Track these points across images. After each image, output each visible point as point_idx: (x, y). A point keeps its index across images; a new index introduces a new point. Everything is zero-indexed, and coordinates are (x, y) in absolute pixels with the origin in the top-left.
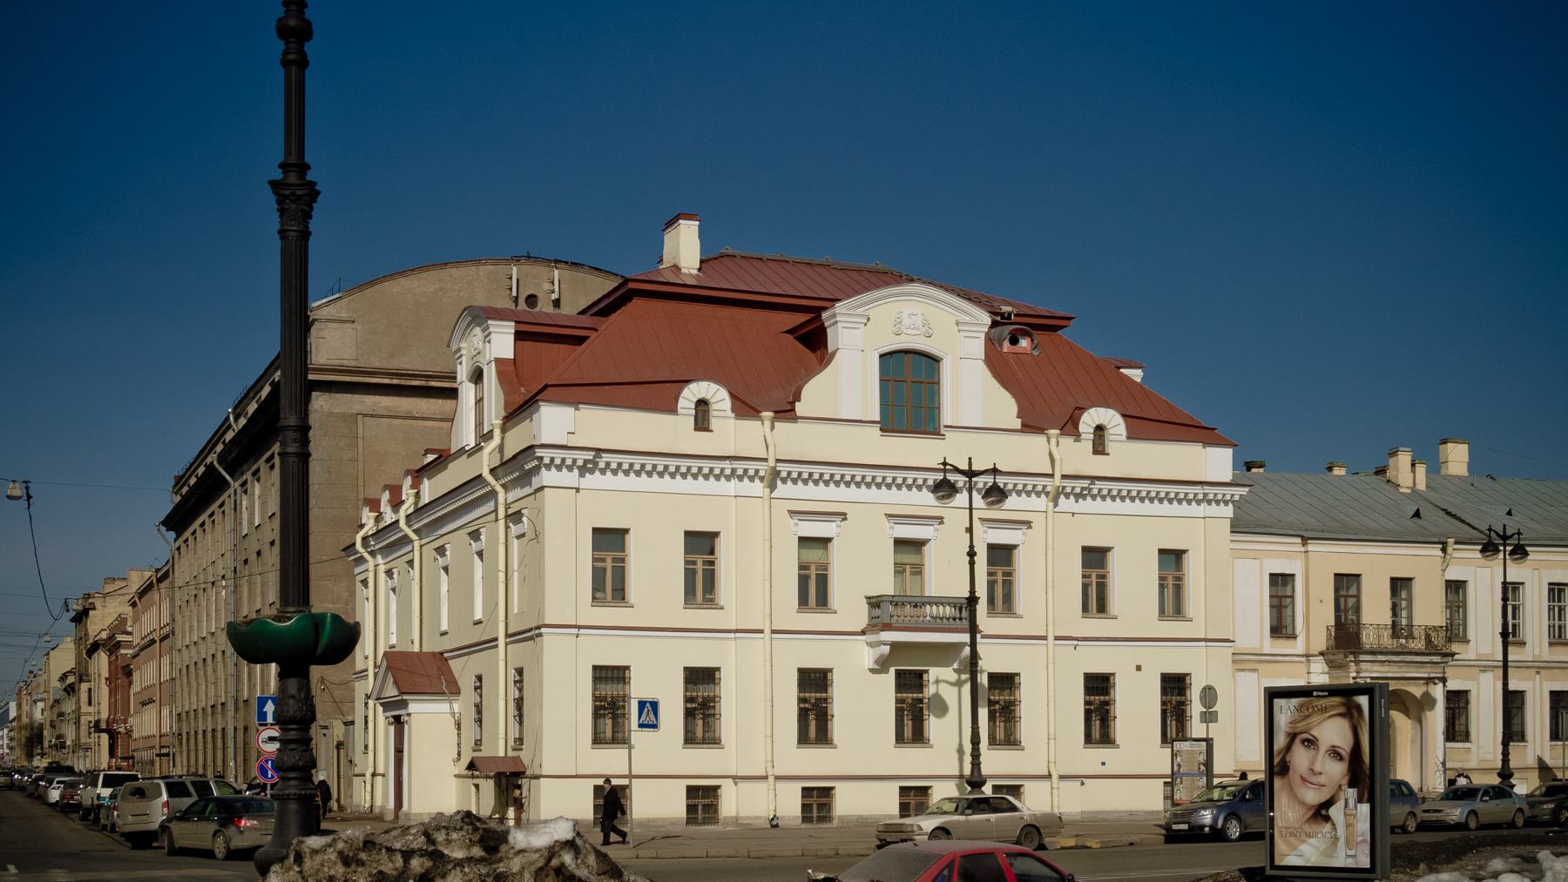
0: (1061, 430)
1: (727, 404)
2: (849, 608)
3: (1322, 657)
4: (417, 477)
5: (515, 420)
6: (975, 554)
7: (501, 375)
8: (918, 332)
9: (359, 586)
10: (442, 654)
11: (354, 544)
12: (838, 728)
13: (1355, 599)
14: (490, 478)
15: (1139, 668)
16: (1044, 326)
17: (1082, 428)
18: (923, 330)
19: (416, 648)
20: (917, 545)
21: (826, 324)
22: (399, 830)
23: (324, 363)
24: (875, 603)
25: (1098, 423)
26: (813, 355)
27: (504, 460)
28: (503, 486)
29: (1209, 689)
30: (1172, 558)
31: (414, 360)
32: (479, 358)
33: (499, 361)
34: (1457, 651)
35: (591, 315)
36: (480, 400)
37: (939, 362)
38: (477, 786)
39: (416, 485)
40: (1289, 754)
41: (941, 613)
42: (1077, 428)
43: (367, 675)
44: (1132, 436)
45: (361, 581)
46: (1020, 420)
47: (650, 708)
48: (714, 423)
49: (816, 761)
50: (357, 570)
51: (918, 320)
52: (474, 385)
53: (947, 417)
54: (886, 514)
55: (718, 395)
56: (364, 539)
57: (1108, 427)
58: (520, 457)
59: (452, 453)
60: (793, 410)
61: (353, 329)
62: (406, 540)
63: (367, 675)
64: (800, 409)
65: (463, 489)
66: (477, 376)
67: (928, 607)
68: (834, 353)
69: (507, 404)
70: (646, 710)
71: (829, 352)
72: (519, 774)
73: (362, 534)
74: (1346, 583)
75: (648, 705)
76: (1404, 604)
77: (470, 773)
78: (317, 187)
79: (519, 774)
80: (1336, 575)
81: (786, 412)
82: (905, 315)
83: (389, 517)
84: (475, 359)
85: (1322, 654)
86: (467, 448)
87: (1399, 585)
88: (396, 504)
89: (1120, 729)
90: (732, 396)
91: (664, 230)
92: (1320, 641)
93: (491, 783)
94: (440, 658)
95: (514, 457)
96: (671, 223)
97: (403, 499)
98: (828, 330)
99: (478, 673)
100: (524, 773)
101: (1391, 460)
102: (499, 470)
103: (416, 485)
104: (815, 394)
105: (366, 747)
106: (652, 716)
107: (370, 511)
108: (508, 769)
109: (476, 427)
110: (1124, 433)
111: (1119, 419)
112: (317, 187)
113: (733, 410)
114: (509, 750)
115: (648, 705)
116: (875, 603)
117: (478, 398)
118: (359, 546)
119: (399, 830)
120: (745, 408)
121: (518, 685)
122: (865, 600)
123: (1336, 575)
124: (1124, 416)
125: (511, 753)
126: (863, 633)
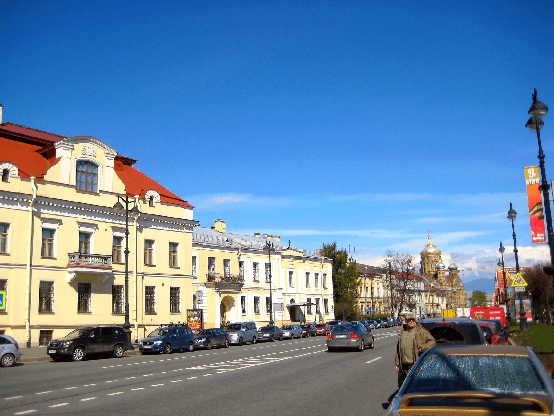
1: (17, 172)
2: (62, 259)
8: (91, 155)
12: (54, 307)
17: (146, 196)
18: (93, 154)
20: (52, 231)
21: (56, 148)
22: (239, 285)
25: (151, 195)
31: (28, 173)
37: (97, 167)
42: (144, 196)
44: (162, 202)
46: (125, 192)
49: (46, 320)
54: (77, 222)
57: (153, 196)
60: (43, 178)
64: (46, 178)
68: (60, 159)
71: (57, 158)
76: (242, 269)
78: (338, 249)
81: (40, 179)
82: (86, 148)
87: (226, 262)
89: (156, 308)
90: (19, 170)
92: (204, 279)
98: (57, 150)
104: (51, 174)
110: (160, 200)
111: (157, 195)
112: (338, 249)
113: (19, 175)
116: (71, 256)
119: (239, 285)
120: (24, 176)
124: (160, 195)
126: (67, 267)
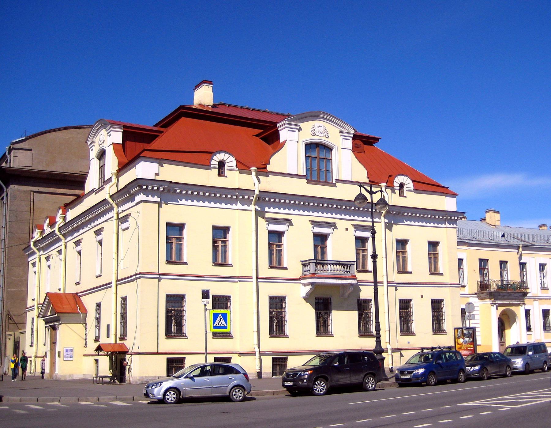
0: (386, 183)
1: (234, 164)
3: (476, 295)
4: (65, 209)
5: (125, 170)
6: (375, 232)
7: (115, 151)
8: (323, 135)
9: (30, 266)
10: (77, 294)
11: (30, 246)
12: (288, 328)
13: (487, 270)
14: (110, 200)
15: (422, 297)
16: (369, 141)
19: (62, 291)
21: (279, 129)
23: (17, 167)
24: (305, 264)
25: (401, 182)
26: (270, 146)
27: (119, 190)
28: (116, 204)
29: (470, 304)
30: (433, 245)
32: (103, 145)
33: (114, 144)
34: (529, 292)
35: (159, 127)
36: (102, 166)
38: (97, 361)
39: (64, 213)
40: (15, 371)
41: (332, 268)
43: (34, 308)
45: (32, 264)
47: (221, 317)
48: (227, 173)
50: (30, 259)
51: (322, 129)
52: (99, 161)
53: (335, 176)
55: (231, 161)
56: (35, 242)
58: (128, 187)
59: (85, 194)
60: (265, 168)
61: (31, 153)
62: (59, 240)
63: (34, 308)
64: (269, 168)
65: (93, 209)
66: (102, 155)
67: (329, 265)
68: (285, 142)
69: (119, 164)
70: (219, 318)
72: (126, 353)
73: (34, 240)
74: (483, 263)
75: (220, 315)
77: (97, 353)
79: (126, 353)
80: (480, 259)
81: (263, 171)
82: (316, 127)
83: (48, 230)
84: (101, 146)
85: (476, 294)
86: (95, 190)
87: (503, 264)
88: (52, 224)
89: (415, 327)
91: (194, 90)
92: (475, 288)
93: (108, 358)
94: (76, 297)
95: (125, 187)
96: (197, 86)
97: (57, 221)
98: (280, 132)
99: (98, 302)
100: (127, 352)
101: (486, 214)
102: (115, 196)
103: (64, 213)
105: (32, 343)
106: (223, 322)
107: (38, 230)
108: (117, 349)
109: (99, 180)
110: (412, 187)
114: (118, 340)
115: (220, 315)
116: (305, 264)
117: (101, 165)
118: (32, 246)
121: (123, 306)
122: (301, 263)
123: (480, 259)
125: (119, 342)
126: (300, 279)
